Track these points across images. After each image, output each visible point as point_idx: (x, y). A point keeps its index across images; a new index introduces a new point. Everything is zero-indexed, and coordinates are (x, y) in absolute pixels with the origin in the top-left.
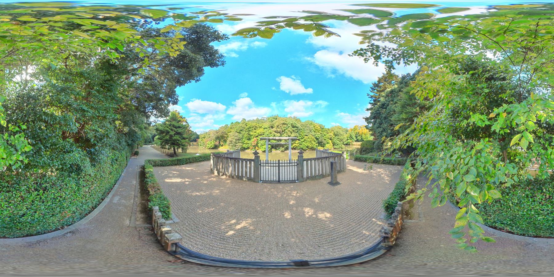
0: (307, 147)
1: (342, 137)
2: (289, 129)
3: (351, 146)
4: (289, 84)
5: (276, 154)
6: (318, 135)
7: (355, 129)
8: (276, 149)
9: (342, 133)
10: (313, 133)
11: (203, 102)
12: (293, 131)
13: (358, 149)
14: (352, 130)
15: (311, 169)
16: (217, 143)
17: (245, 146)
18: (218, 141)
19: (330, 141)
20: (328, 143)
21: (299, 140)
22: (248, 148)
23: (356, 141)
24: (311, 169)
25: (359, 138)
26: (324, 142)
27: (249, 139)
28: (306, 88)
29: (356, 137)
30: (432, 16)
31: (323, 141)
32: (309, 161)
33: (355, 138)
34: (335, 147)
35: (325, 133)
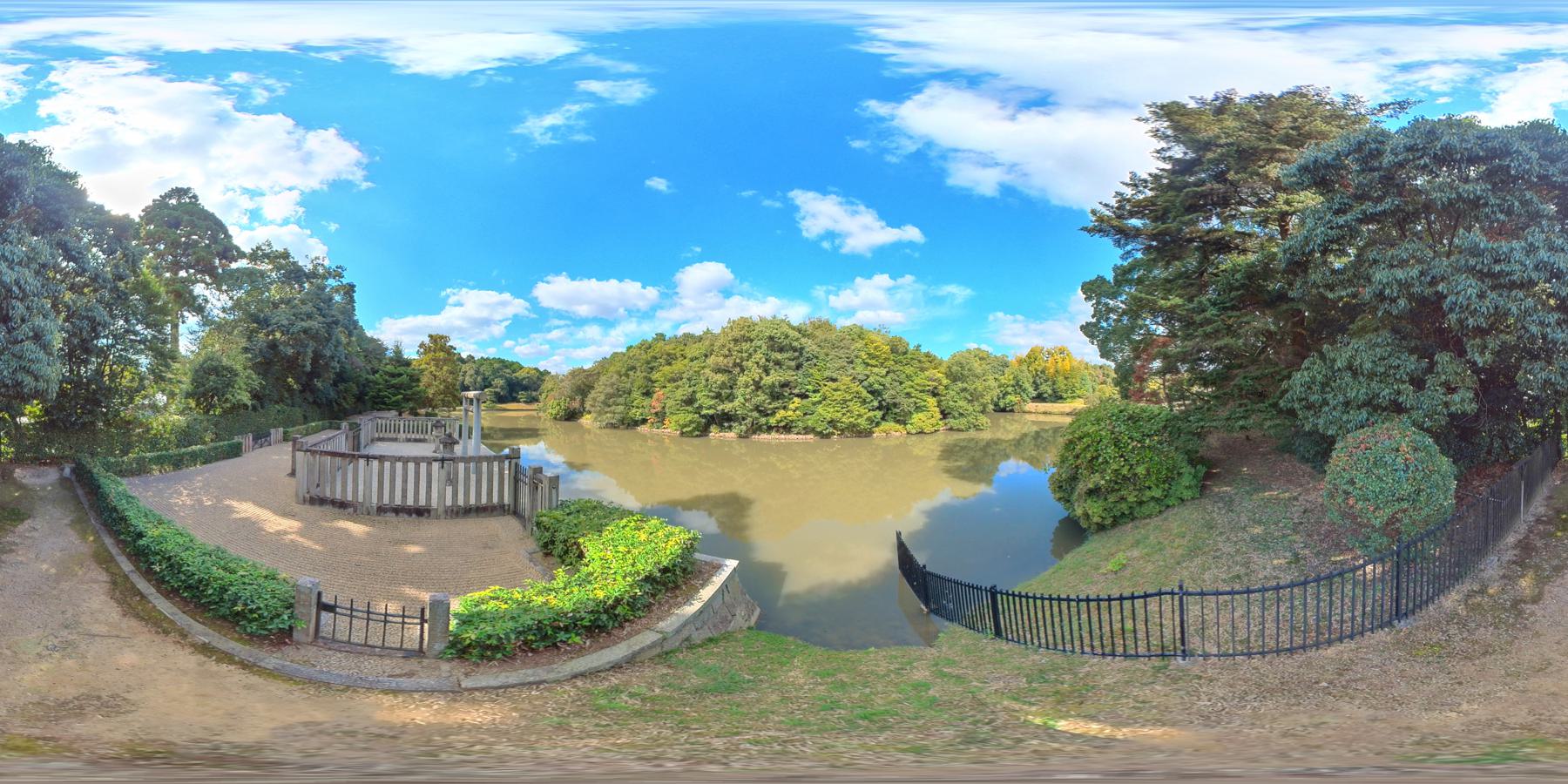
0: (832, 423)
1: (979, 385)
2: (758, 356)
3: (1017, 416)
4: (821, 212)
5: (723, 443)
6: (877, 375)
7: (1032, 357)
8: (721, 426)
9: (979, 371)
10: (860, 369)
11: (576, 284)
12: (778, 363)
13: (1057, 430)
14: (1020, 362)
15: (479, 482)
16: (576, 405)
17: (636, 414)
18: (578, 398)
19: (932, 401)
20: (918, 409)
21: (803, 396)
22: (644, 421)
23: (1035, 399)
24: (479, 482)
25: (1046, 388)
26: (906, 404)
27: (648, 394)
28: (894, 221)
29: (1036, 386)
30: (858, 40)
31: (901, 399)
32: (485, 464)
33: (1030, 389)
34: (952, 422)
35: (909, 370)
